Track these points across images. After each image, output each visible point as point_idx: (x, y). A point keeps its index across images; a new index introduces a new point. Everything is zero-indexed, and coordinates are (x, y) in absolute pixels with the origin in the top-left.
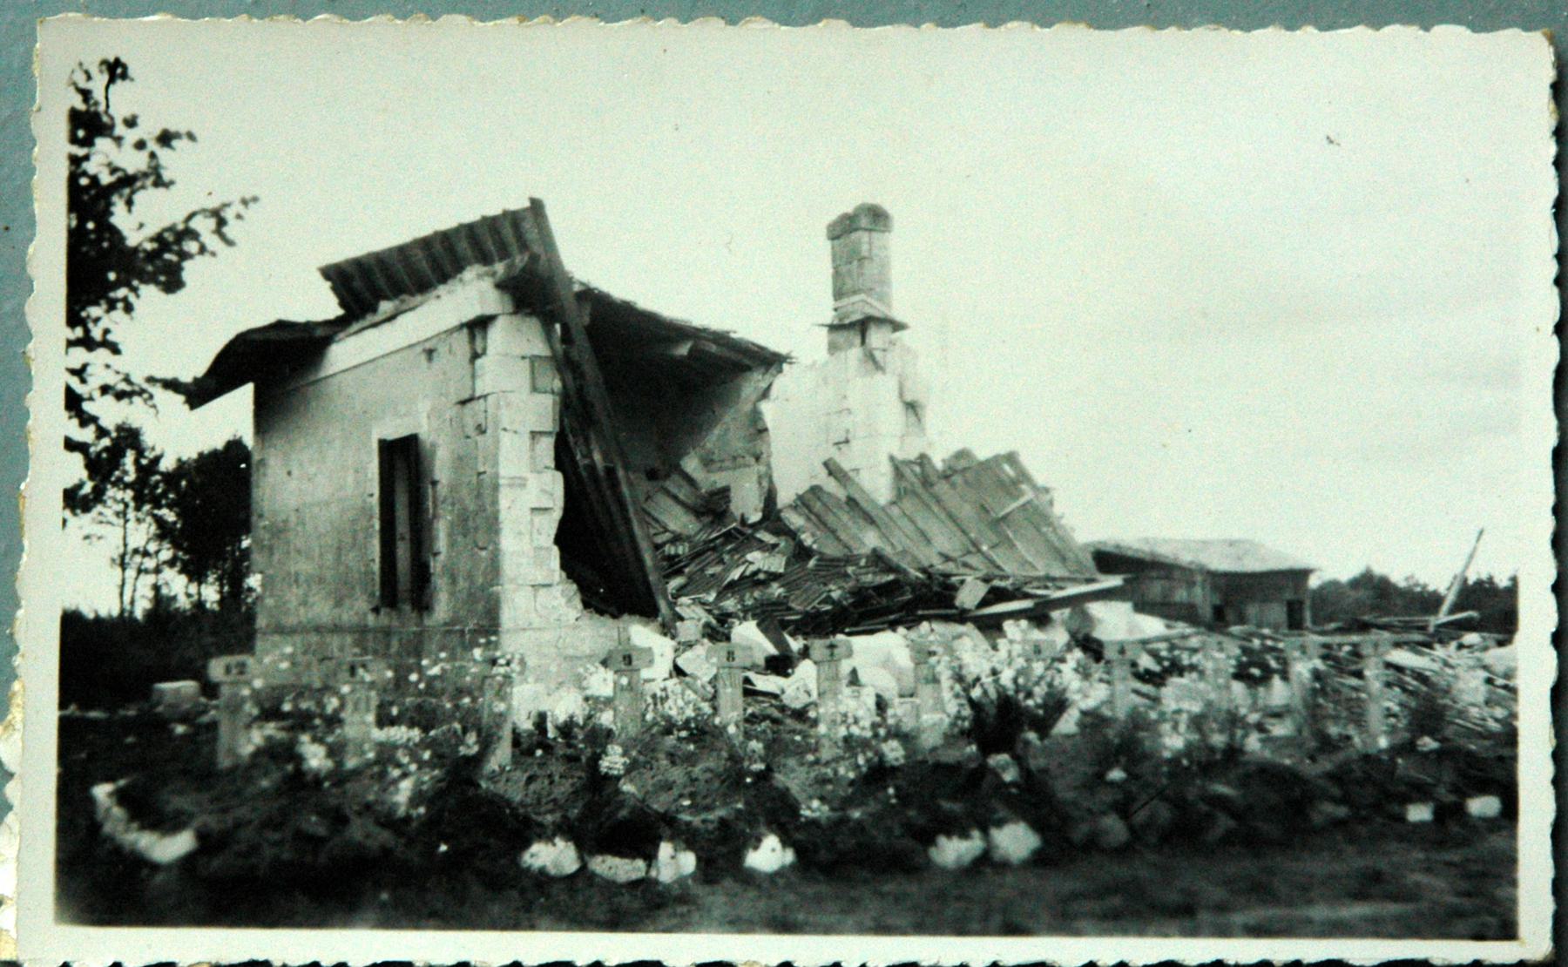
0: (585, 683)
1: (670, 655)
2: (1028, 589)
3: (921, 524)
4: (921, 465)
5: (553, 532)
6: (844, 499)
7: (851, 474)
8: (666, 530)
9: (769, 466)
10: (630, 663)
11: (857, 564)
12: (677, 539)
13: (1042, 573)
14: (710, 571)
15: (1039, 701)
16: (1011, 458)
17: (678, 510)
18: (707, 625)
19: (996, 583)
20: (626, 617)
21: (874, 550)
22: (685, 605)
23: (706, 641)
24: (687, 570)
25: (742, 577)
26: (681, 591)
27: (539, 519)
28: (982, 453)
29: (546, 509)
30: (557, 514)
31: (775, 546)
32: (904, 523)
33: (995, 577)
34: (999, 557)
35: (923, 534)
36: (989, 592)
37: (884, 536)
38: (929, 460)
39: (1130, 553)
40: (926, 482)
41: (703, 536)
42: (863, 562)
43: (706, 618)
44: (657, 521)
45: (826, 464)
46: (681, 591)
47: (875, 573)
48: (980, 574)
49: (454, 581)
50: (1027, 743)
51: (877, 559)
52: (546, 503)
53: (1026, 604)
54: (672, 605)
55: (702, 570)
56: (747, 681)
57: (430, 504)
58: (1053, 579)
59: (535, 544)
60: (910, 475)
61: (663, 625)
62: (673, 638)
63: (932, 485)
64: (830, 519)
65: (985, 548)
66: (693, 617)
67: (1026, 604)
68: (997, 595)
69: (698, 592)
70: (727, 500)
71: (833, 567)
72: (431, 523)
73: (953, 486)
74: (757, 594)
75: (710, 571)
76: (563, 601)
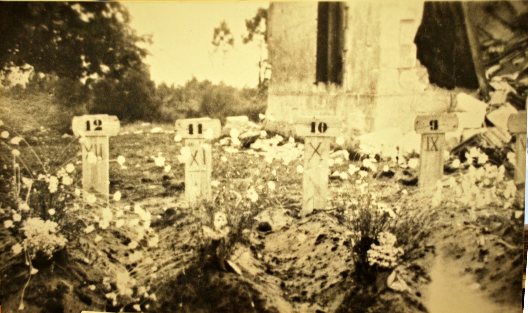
1: (484, 113)
10: (436, 127)
12: (498, 43)
14: (516, 61)
18: (511, 94)
20: (456, 89)
22: (497, 83)
23: (508, 104)
26: (495, 74)
27: (405, 26)
39: (464, 89)
41: (514, 41)
43: (509, 89)
44: (487, 33)
46: (495, 74)
49: (353, 66)
52: (410, 16)
54: (487, 82)
55: (511, 61)
62: (487, 101)
66: (501, 88)
69: (506, 73)
72: (344, 31)
75: (516, 61)
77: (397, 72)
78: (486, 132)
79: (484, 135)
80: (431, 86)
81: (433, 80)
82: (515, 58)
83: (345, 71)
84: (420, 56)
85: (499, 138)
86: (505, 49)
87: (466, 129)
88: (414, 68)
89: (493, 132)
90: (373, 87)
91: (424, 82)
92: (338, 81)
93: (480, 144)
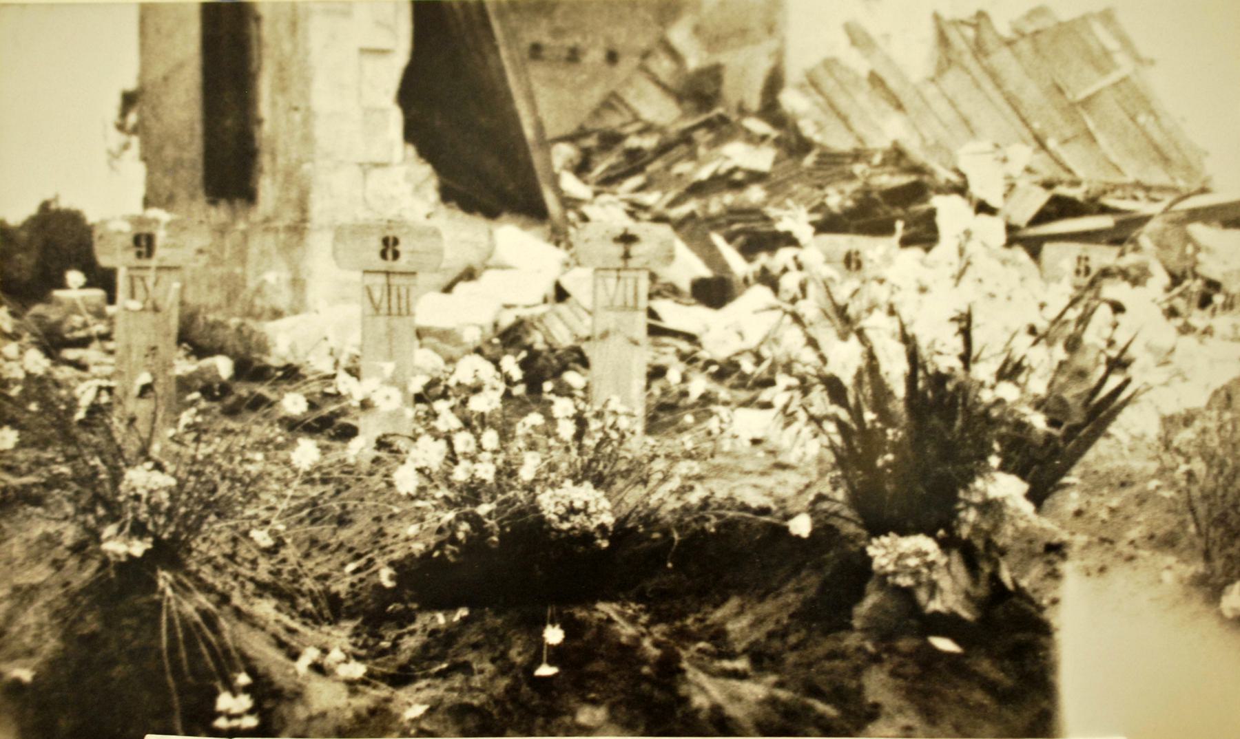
0: (257, 310)
2: (1109, 201)
4: (976, 27)
9: (783, 40)
11: (869, 163)
12: (648, 129)
13: (1130, 178)
17: (653, 92)
19: (1063, 190)
27: (370, 64)
31: (764, 138)
32: (941, 107)
33: (1061, 182)
34: (1073, 156)
35: (966, 122)
42: (877, 159)
48: (1039, 178)
49: (274, 159)
51: (897, 156)
52: (381, 41)
53: (1105, 222)
55: (668, 168)
56: (652, 314)
58: (1148, 189)
60: (961, 40)
61: (555, 230)
63: (987, 54)
64: (842, 102)
67: (1105, 222)
68: (1060, 208)
73: (1017, 56)
76: (408, 188)
77: (356, 171)
78: (544, 315)
79: (540, 320)
81: (447, 195)
82: (678, 160)
83: (261, 171)
84: (412, 133)
85: (570, 328)
87: (508, 307)
89: (559, 315)
90: (303, 207)
91: (425, 198)
92: (249, 196)
93: (528, 340)
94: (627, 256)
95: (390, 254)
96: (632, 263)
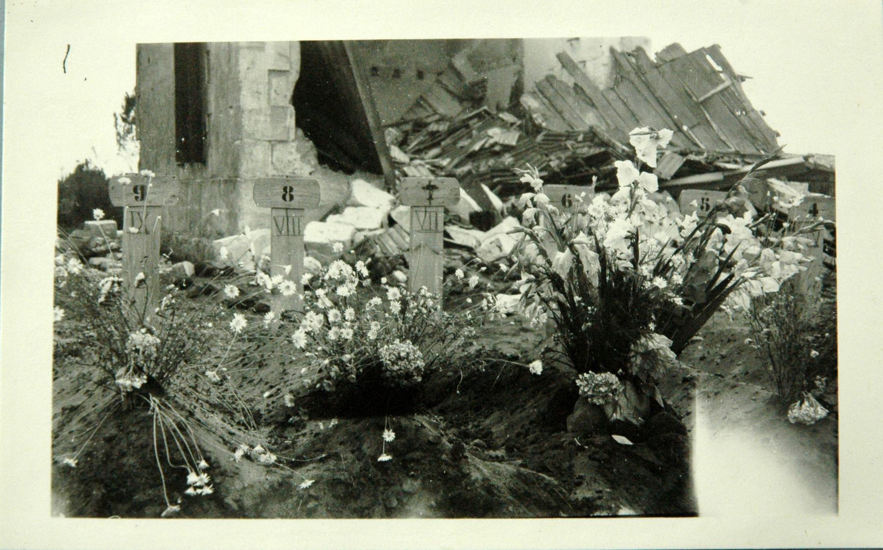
3: (632, 106)
5: (289, 93)
6: (571, 84)
7: (580, 66)
8: (435, 113)
13: (733, 150)
15: (678, 279)
16: (714, 51)
19: (692, 157)
21: (591, 128)
24: (443, 143)
25: (482, 149)
28: (689, 47)
29: (285, 71)
30: (294, 77)
31: (512, 124)
36: (685, 164)
37: (602, 118)
38: (644, 52)
40: (639, 71)
42: (580, 138)
44: (430, 106)
45: (559, 56)
47: (590, 147)
49: (218, 138)
50: (651, 356)
55: (455, 143)
56: (446, 235)
57: (206, 71)
58: (743, 156)
59: (273, 103)
64: (559, 103)
65: (685, 128)
70: (484, 89)
71: (555, 141)
73: (662, 74)
74: (491, 162)
76: (299, 156)
80: (319, 167)
81: (322, 160)
82: (460, 138)
86: (449, 127)
88: (293, 141)
89: (390, 235)
94: (431, 198)
95: (288, 197)
96: (434, 203)
